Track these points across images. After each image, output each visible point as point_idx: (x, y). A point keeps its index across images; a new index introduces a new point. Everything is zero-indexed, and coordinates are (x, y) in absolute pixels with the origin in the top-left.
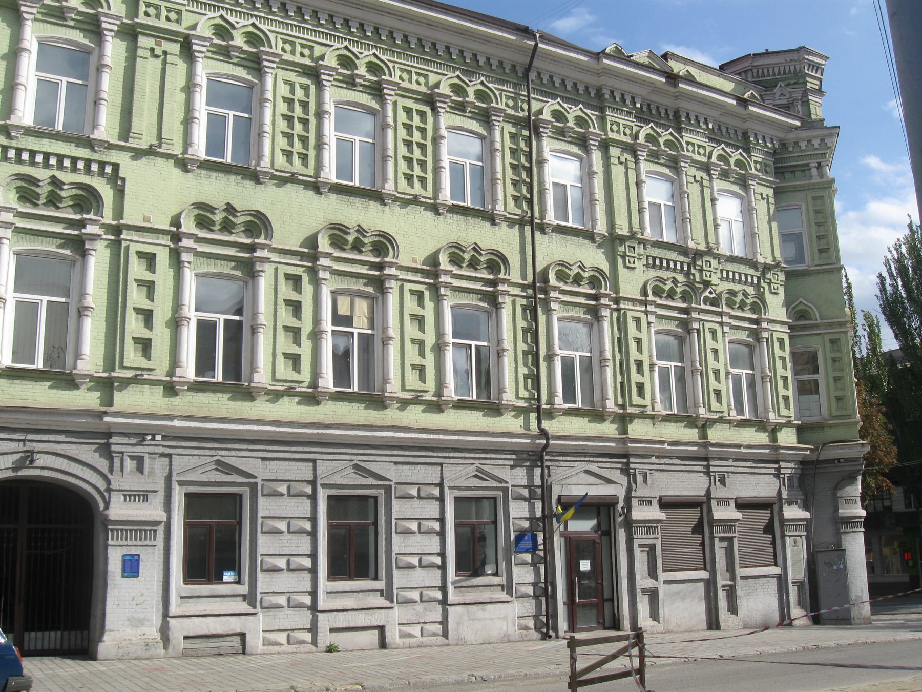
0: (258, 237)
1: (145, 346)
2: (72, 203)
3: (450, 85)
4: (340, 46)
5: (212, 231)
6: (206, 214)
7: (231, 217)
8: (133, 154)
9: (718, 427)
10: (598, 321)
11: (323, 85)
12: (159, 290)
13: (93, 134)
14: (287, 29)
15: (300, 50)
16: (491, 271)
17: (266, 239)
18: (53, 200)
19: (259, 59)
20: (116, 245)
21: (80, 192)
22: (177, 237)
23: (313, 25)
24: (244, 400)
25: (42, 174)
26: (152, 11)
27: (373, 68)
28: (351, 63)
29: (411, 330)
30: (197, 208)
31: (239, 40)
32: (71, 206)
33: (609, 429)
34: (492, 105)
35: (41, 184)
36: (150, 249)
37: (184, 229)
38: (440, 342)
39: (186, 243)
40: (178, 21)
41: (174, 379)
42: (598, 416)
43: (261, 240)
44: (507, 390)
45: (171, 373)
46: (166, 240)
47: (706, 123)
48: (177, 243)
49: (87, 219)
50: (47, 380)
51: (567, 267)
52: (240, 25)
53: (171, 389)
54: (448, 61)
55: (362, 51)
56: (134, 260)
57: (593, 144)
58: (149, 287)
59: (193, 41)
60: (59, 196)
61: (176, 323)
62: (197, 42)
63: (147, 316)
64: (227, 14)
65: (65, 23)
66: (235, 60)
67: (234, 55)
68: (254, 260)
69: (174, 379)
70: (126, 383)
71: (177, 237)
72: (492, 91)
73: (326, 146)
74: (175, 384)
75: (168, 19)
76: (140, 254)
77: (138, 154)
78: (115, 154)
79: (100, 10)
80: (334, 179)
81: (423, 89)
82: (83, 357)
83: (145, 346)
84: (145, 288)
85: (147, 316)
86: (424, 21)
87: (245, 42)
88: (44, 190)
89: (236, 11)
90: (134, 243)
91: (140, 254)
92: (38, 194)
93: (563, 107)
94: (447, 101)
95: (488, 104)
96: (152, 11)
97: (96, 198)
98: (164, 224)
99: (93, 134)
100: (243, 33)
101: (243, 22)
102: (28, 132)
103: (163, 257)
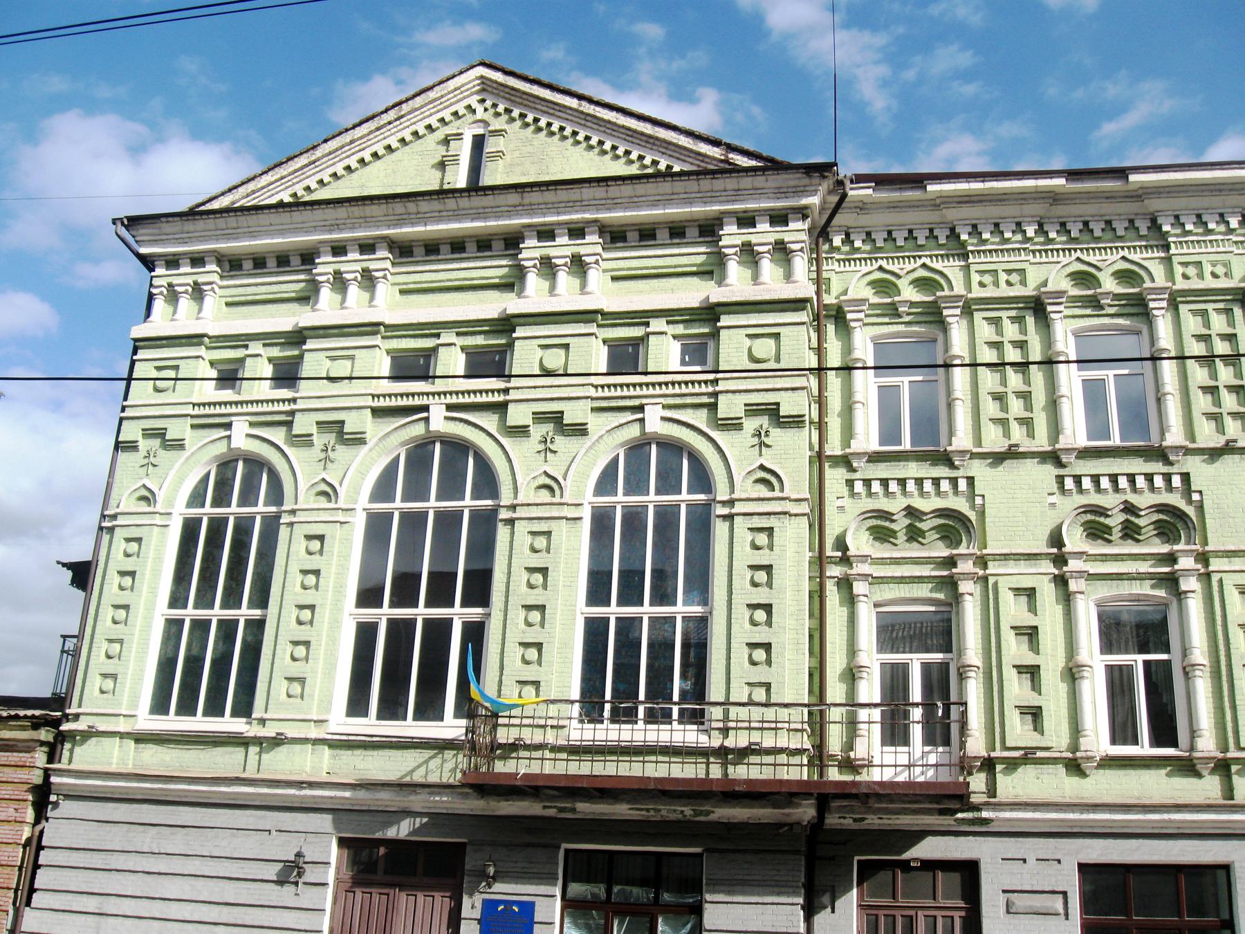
0: (1177, 540)
1: (1035, 714)
2: (1156, 532)
3: (1113, 274)
4: (869, 268)
5: (1109, 541)
6: (1097, 519)
7: (1133, 519)
8: (991, 460)
9: (1027, 773)
10: (1180, 600)
11: (1154, 315)
12: (1045, 638)
13: (951, 445)
14: (1015, 256)
15: (1181, 272)
16: (948, 542)
17: (1188, 543)
18: (1130, 532)
19: (1144, 300)
20: (1206, 577)
21: (1162, 517)
22: (1060, 560)
23: (1064, 243)
24: (1187, 776)
25: (1110, 501)
26: (1220, 270)
27: (1124, 276)
28: (1134, 277)
29: (1014, 650)
30: (1158, 511)
31: (1109, 284)
32: (1155, 535)
33: (1208, 787)
34: (1145, 286)
35: (894, 518)
36: (1027, 583)
37: (1069, 548)
38: (852, 666)
39: (861, 568)
40: (1023, 283)
41: (1078, 754)
42: (1187, 767)
43: (962, 550)
44: (1204, 733)
45: (1074, 747)
46: (1049, 568)
47: (1222, 219)
48: (1173, 566)
49: (1178, 551)
50: (1165, 766)
51: (887, 519)
52: (905, 271)
53: (1075, 767)
54: (914, 251)
55: (1104, 257)
56: (1007, 598)
57: (1158, 306)
58: (1031, 634)
59: (846, 309)
60: (920, 530)
61: (1072, 674)
62: (1154, 297)
63: (1032, 672)
64: (932, 261)
65: (900, 320)
66: (907, 319)
67: (904, 312)
68: (1176, 575)
69: (1078, 754)
70: (1012, 765)
71: (1060, 560)
72: (941, 273)
73: (1064, 400)
74: (1195, 761)
75: (1214, 275)
76: (1017, 591)
77: (1214, 454)
78: (1230, 461)
79: (938, 294)
80: (1082, 441)
81: (1017, 291)
82: (1085, 733)
83: (1035, 714)
84: (1026, 638)
85: (1032, 672)
86: (1100, 195)
87: (876, 293)
88: (1115, 520)
89: (1186, 242)
90: (1007, 576)
91: (1017, 591)
92: (1110, 528)
93: (1089, 264)
94: (864, 308)
95: (1140, 286)
96: (1191, 271)
97: (1182, 519)
98: (1040, 545)
99: (951, 445)
100: (1069, 275)
101: (909, 266)
102: (1086, 454)
103: (1047, 593)
